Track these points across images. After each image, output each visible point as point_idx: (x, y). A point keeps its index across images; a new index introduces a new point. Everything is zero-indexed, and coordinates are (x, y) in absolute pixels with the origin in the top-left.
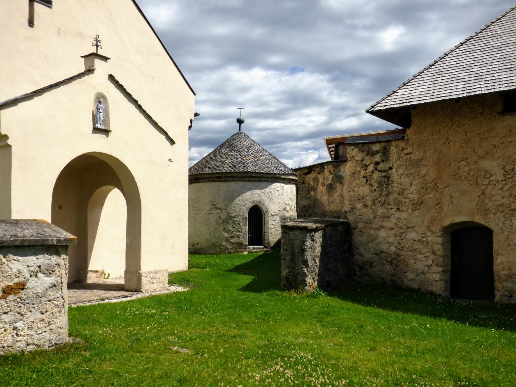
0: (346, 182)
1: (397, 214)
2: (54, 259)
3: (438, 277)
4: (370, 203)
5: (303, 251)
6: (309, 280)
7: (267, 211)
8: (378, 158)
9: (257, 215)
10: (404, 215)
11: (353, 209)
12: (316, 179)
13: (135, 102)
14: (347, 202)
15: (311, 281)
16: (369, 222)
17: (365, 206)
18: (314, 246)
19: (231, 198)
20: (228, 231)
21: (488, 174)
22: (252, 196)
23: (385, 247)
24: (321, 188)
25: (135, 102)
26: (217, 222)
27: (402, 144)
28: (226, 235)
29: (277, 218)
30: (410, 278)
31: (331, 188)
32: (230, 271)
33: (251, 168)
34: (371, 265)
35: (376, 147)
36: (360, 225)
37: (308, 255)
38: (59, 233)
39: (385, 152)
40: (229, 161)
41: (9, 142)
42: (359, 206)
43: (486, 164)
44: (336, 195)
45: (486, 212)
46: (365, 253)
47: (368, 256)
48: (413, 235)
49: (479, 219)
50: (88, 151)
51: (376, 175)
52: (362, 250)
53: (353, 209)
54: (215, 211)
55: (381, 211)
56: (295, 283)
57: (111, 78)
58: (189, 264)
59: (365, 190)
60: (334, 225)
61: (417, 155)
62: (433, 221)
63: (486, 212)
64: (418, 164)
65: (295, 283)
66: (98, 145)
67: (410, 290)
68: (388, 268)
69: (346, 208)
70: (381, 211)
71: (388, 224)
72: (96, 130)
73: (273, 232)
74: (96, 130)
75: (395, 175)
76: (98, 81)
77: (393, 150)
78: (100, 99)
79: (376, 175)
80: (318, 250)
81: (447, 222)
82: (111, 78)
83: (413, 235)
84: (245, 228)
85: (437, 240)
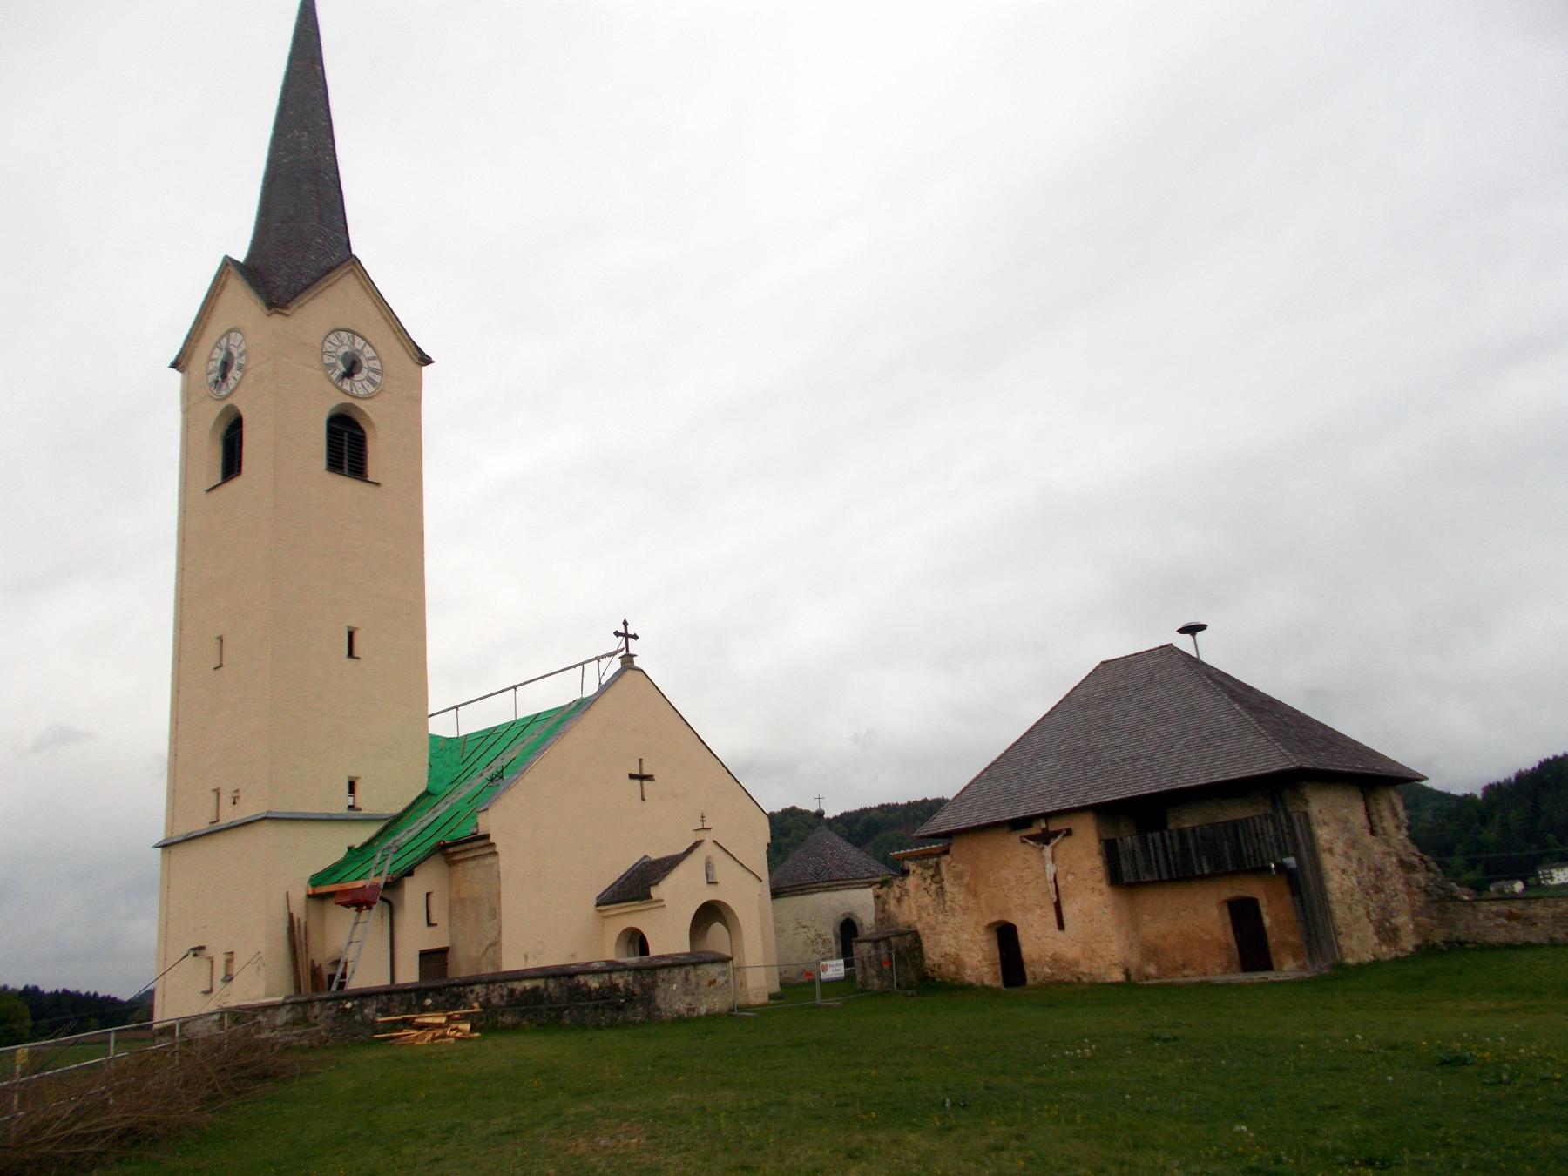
0: (911, 894)
2: (1295, 816)
23: (947, 949)
24: (893, 902)
30: (969, 975)
31: (899, 900)
32: (300, 236)
38: (1498, 914)
41: (492, 840)
48: (966, 936)
51: (934, 887)
54: (801, 931)
58: (772, 831)
59: (927, 900)
61: (960, 867)
66: (710, 894)
70: (941, 917)
71: (947, 929)
75: (946, 885)
76: (707, 849)
77: (943, 866)
78: (708, 866)
79: (934, 887)
83: (966, 936)
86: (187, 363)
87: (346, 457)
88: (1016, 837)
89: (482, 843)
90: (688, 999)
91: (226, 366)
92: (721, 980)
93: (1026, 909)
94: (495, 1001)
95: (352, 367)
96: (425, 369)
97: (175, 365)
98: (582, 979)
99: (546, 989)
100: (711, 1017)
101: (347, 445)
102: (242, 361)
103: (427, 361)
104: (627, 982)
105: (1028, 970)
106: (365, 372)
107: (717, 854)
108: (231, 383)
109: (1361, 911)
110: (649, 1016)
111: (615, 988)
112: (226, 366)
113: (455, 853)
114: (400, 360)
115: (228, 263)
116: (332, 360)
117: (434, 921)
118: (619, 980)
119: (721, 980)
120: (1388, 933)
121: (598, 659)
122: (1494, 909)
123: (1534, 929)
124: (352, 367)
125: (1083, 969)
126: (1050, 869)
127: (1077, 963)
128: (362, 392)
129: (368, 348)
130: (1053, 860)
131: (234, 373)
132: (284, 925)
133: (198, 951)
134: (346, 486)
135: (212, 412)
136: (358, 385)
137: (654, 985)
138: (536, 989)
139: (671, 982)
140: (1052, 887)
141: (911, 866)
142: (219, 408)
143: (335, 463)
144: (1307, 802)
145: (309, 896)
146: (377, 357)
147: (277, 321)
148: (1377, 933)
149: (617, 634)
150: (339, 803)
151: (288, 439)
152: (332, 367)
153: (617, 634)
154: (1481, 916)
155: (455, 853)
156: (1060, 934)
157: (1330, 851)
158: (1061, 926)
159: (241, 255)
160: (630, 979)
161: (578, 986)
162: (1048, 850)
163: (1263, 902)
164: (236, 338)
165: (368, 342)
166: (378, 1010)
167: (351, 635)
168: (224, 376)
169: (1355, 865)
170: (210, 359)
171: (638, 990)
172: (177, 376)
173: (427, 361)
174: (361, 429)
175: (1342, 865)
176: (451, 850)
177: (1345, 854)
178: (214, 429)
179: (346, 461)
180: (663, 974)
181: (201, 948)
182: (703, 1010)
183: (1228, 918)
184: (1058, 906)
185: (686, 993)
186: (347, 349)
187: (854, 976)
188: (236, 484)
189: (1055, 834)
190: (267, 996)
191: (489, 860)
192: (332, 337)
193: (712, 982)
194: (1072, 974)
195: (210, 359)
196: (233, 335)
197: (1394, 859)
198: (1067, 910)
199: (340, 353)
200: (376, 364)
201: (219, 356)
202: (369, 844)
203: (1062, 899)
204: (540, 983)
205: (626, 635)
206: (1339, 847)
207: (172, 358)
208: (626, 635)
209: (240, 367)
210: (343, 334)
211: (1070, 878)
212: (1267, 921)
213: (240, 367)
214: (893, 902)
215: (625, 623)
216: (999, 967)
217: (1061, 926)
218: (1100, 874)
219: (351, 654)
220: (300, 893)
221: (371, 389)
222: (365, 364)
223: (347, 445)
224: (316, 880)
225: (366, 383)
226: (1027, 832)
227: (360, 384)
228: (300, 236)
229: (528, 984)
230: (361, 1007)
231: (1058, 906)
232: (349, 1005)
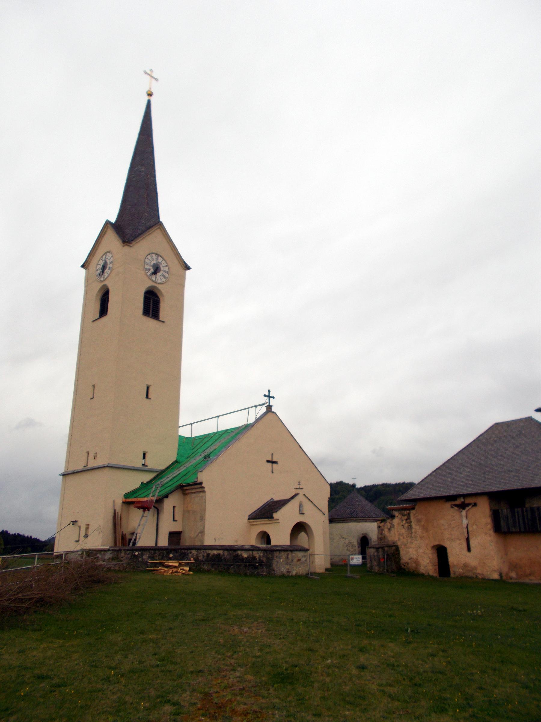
1: (415, 542)
4: (405, 537)
7: (371, 539)
14: (397, 536)
17: (404, 538)
23: (412, 556)
30: (422, 569)
31: (389, 529)
32: (139, 212)
36: (403, 546)
42: (401, 538)
44: (392, 532)
50: (313, 530)
51: (407, 525)
52: (404, 558)
53: (399, 539)
54: (342, 540)
59: (403, 531)
66: (301, 519)
67: (423, 575)
69: (397, 539)
70: (409, 540)
71: (412, 546)
74: (300, 513)
76: (300, 498)
79: (407, 525)
81: (432, 545)
86: (88, 266)
88: (448, 505)
89: (199, 486)
90: (287, 567)
91: (104, 268)
92: (303, 559)
94: (201, 558)
95: (156, 270)
96: (188, 272)
97: (83, 266)
99: (224, 555)
101: (152, 304)
102: (111, 266)
103: (188, 268)
104: (260, 556)
106: (161, 272)
107: (305, 500)
108: (106, 275)
110: (269, 573)
111: (254, 558)
112: (104, 268)
114: (176, 267)
115: (108, 223)
117: (176, 519)
118: (257, 554)
119: (303, 559)
121: (256, 406)
124: (156, 270)
126: (465, 522)
127: (476, 568)
128: (160, 281)
129: (164, 262)
130: (467, 517)
131: (107, 271)
132: (112, 514)
133: (74, 522)
134: (150, 322)
135: (97, 287)
136: (158, 278)
137: (272, 559)
138: (219, 554)
139: (280, 558)
140: (465, 530)
142: (100, 285)
145: (123, 502)
146: (167, 266)
147: (127, 249)
149: (265, 396)
150: (138, 463)
151: (127, 300)
152: (148, 269)
156: (468, 554)
158: (469, 549)
159: (113, 220)
160: (262, 554)
161: (238, 556)
162: (464, 513)
164: (109, 256)
165: (164, 259)
167: (148, 388)
168: (103, 272)
170: (98, 264)
171: (264, 560)
172: (83, 271)
173: (188, 268)
174: (158, 297)
176: (185, 488)
178: (97, 295)
179: (151, 311)
180: (277, 554)
181: (76, 521)
182: (294, 573)
184: (468, 540)
185: (287, 564)
186: (154, 262)
188: (105, 319)
189: (468, 505)
192: (149, 257)
193: (299, 560)
195: (98, 264)
198: (472, 542)
199: (152, 263)
200: (166, 269)
201: (102, 263)
202: (148, 483)
203: (470, 537)
204: (221, 552)
205: (269, 397)
207: (82, 263)
208: (269, 397)
209: (110, 268)
210: (154, 255)
213: (110, 268)
215: (269, 391)
216: (437, 567)
217: (469, 549)
219: (147, 397)
220: (119, 501)
221: (164, 280)
222: (162, 269)
223: (152, 304)
224: (127, 495)
225: (162, 277)
226: (453, 503)
227: (159, 278)
228: (139, 212)
230: (142, 555)
231: (468, 540)
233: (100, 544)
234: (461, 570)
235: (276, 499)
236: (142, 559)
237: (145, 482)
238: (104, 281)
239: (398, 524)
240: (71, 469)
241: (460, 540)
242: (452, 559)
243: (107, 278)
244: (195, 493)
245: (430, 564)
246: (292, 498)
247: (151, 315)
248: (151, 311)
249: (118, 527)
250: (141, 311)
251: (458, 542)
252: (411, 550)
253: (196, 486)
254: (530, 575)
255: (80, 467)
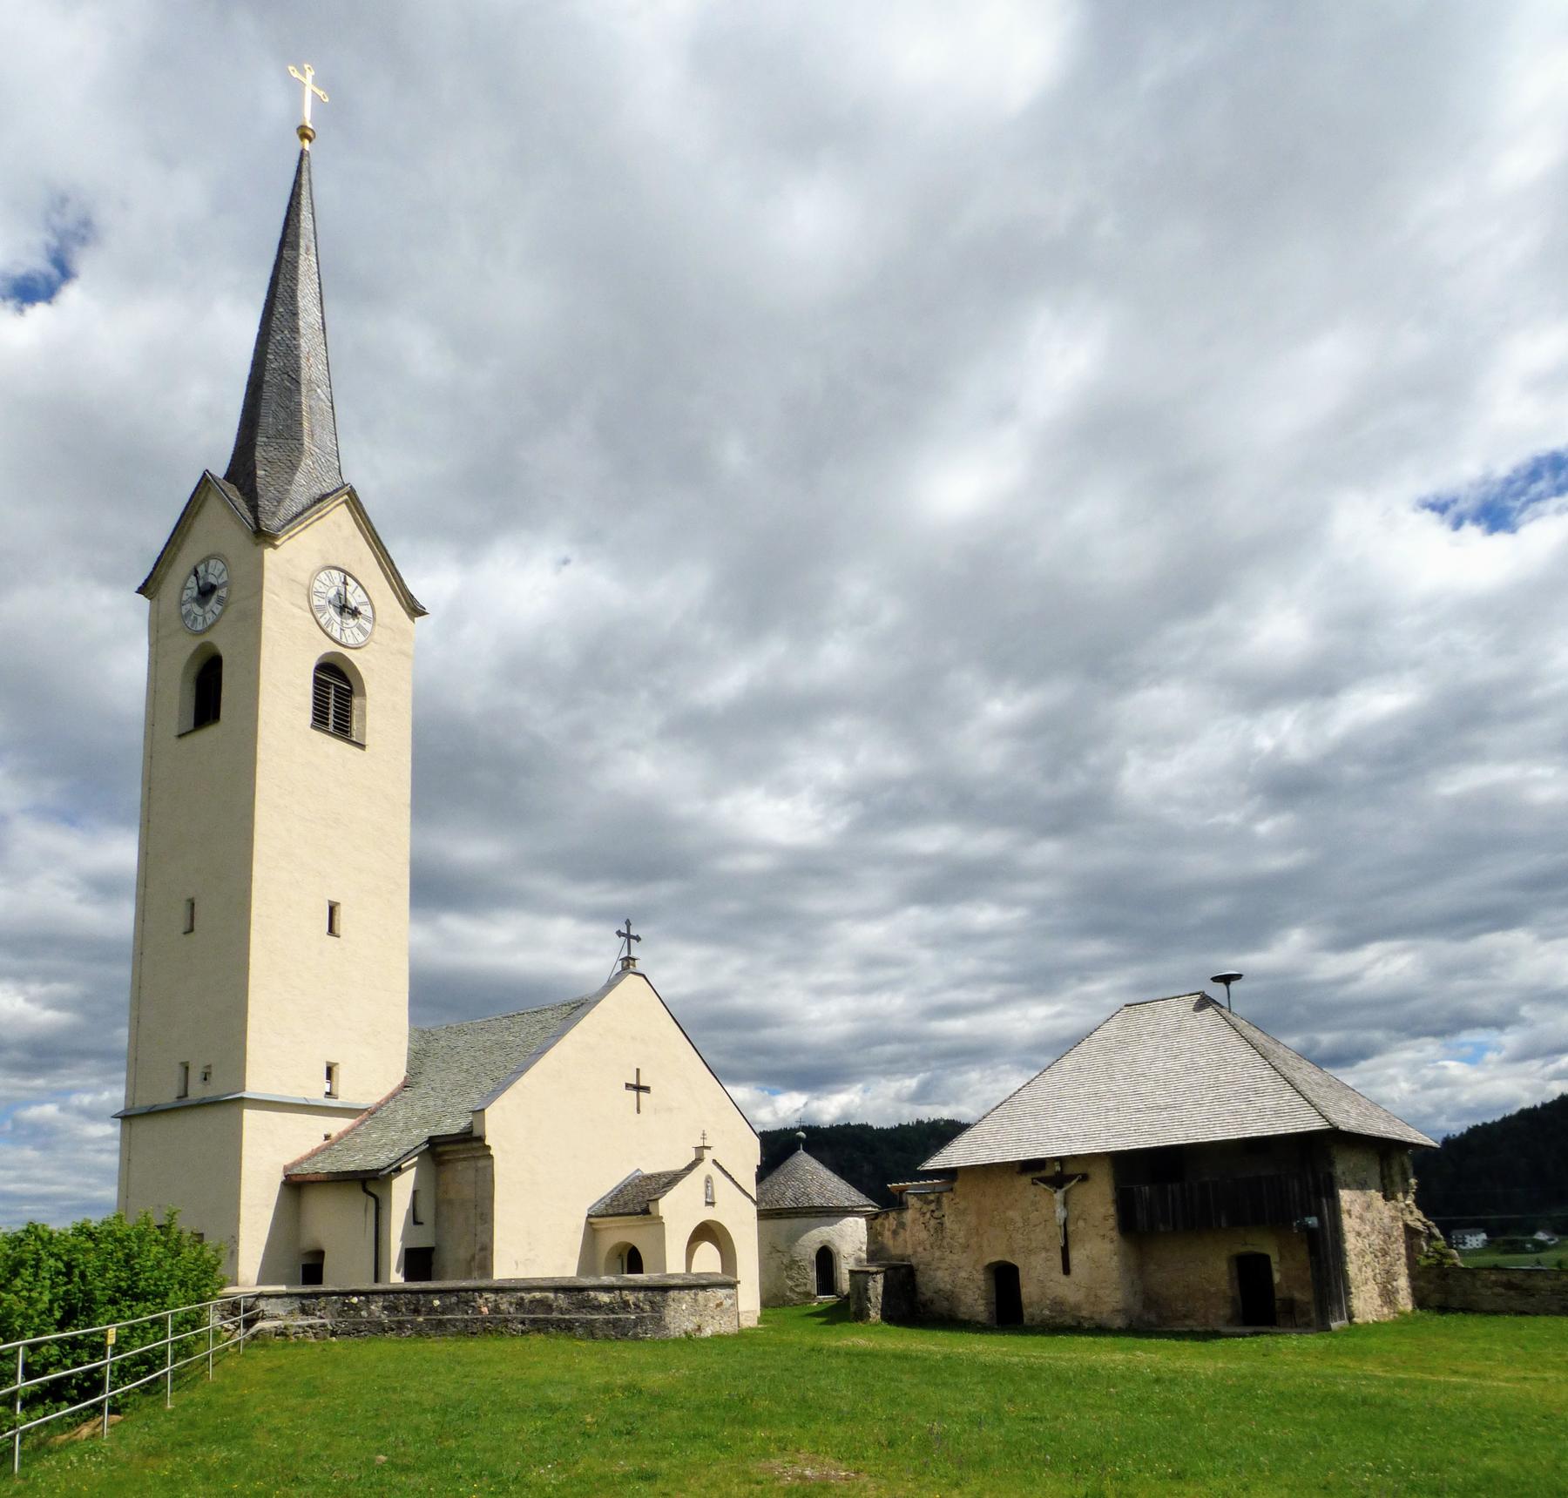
3: (982, 1308)
5: (867, 1290)
6: (872, 1313)
8: (933, 1207)
9: (826, 1258)
10: (955, 1257)
11: (915, 1252)
12: (882, 1225)
13: (729, 1176)
15: (875, 1314)
16: (928, 1264)
18: (877, 1287)
19: (793, 1238)
20: (791, 1278)
21: (1012, 1221)
22: (819, 1234)
23: (942, 1286)
24: (887, 1234)
25: (729, 1176)
26: (779, 1268)
27: (951, 1195)
28: (790, 1283)
29: (852, 1261)
30: (963, 1313)
31: (895, 1233)
33: (818, 1202)
34: (932, 1302)
35: (931, 1197)
37: (871, 1293)
38: (1495, 1283)
39: (938, 1201)
40: (789, 1193)
42: (920, 1249)
43: (1010, 1213)
44: (900, 1239)
45: (1012, 1252)
46: (926, 1292)
47: (929, 1294)
48: (963, 1274)
49: (1009, 1259)
51: (933, 1222)
53: (915, 1252)
55: (938, 1254)
56: (861, 1315)
57: (715, 1162)
59: (924, 1235)
60: (895, 1268)
61: (962, 1205)
62: (976, 1261)
63: (1012, 1252)
64: (964, 1212)
65: (861, 1315)
66: (708, 1214)
68: (945, 1303)
69: (910, 1251)
70: (938, 1254)
71: (944, 1266)
72: (708, 1203)
73: (844, 1268)
76: (706, 1167)
77: (945, 1200)
78: (708, 1180)
79: (933, 1222)
80: (880, 1289)
81: (987, 1262)
82: (715, 1162)
84: (813, 1275)
85: (980, 1277)
86: (157, 589)
87: (332, 712)
88: (1026, 1179)
89: (475, 1145)
90: (696, 1320)
93: (1030, 1252)
97: (141, 591)
98: (592, 1294)
100: (719, 1338)
105: (1027, 1312)
109: (1370, 1274)
113: (446, 1153)
115: (205, 481)
116: (323, 602)
117: (421, 1218)
119: (727, 1303)
120: (1388, 1296)
122: (1493, 1278)
123: (1532, 1300)
125: (1084, 1313)
126: (1060, 1213)
127: (1077, 1307)
128: (351, 641)
130: (1065, 1204)
135: (184, 649)
139: (680, 1301)
140: (1061, 1232)
141: (912, 1201)
142: (192, 644)
143: (320, 720)
144: (1332, 1164)
148: (1381, 1295)
149: (638, 939)
150: (315, 1090)
153: (638, 939)
154: (1479, 1283)
155: (446, 1153)
156: (1063, 1278)
157: (1349, 1212)
158: (1066, 1270)
162: (1059, 1196)
163: (1274, 1259)
166: (385, 1308)
169: (1368, 1228)
170: (184, 588)
172: (144, 602)
175: (1357, 1228)
176: (440, 1149)
177: (1361, 1218)
178: (186, 672)
179: (331, 717)
180: (673, 1294)
183: (1235, 1274)
184: (1065, 1252)
187: (848, 1307)
188: (210, 733)
189: (1070, 1178)
190: (259, 1283)
191: (482, 1163)
192: (323, 576)
193: (720, 1304)
194: (1074, 1317)
195: (184, 588)
196: (212, 562)
197: (1400, 1224)
198: (1076, 1256)
203: (1071, 1243)
206: (1356, 1209)
207: (140, 583)
210: (335, 573)
211: (1081, 1223)
212: (1277, 1278)
214: (887, 1234)
215: (628, 924)
216: (993, 1307)
217: (1066, 1270)
218: (1112, 1222)
219: (331, 931)
221: (361, 638)
225: (355, 630)
226: (1038, 1175)
229: (538, 1295)
230: (368, 1302)
231: (1065, 1252)
232: (355, 1300)
233: (255, 1280)
234: (1047, 1312)
235: (649, 1169)
236: (370, 1314)
237: (334, 1135)
238: (202, 633)
239: (914, 1221)
240: (145, 1102)
241: (1047, 1250)
242: (1029, 1291)
243: (212, 625)
244: (465, 1159)
245: (981, 1302)
246: (690, 1168)
247: (331, 728)
248: (331, 717)
249: (714, 1279)
250: (307, 716)
251: (1044, 1254)
252: (939, 1274)
253: (469, 1145)
254: (1185, 1317)
255: (168, 1097)
